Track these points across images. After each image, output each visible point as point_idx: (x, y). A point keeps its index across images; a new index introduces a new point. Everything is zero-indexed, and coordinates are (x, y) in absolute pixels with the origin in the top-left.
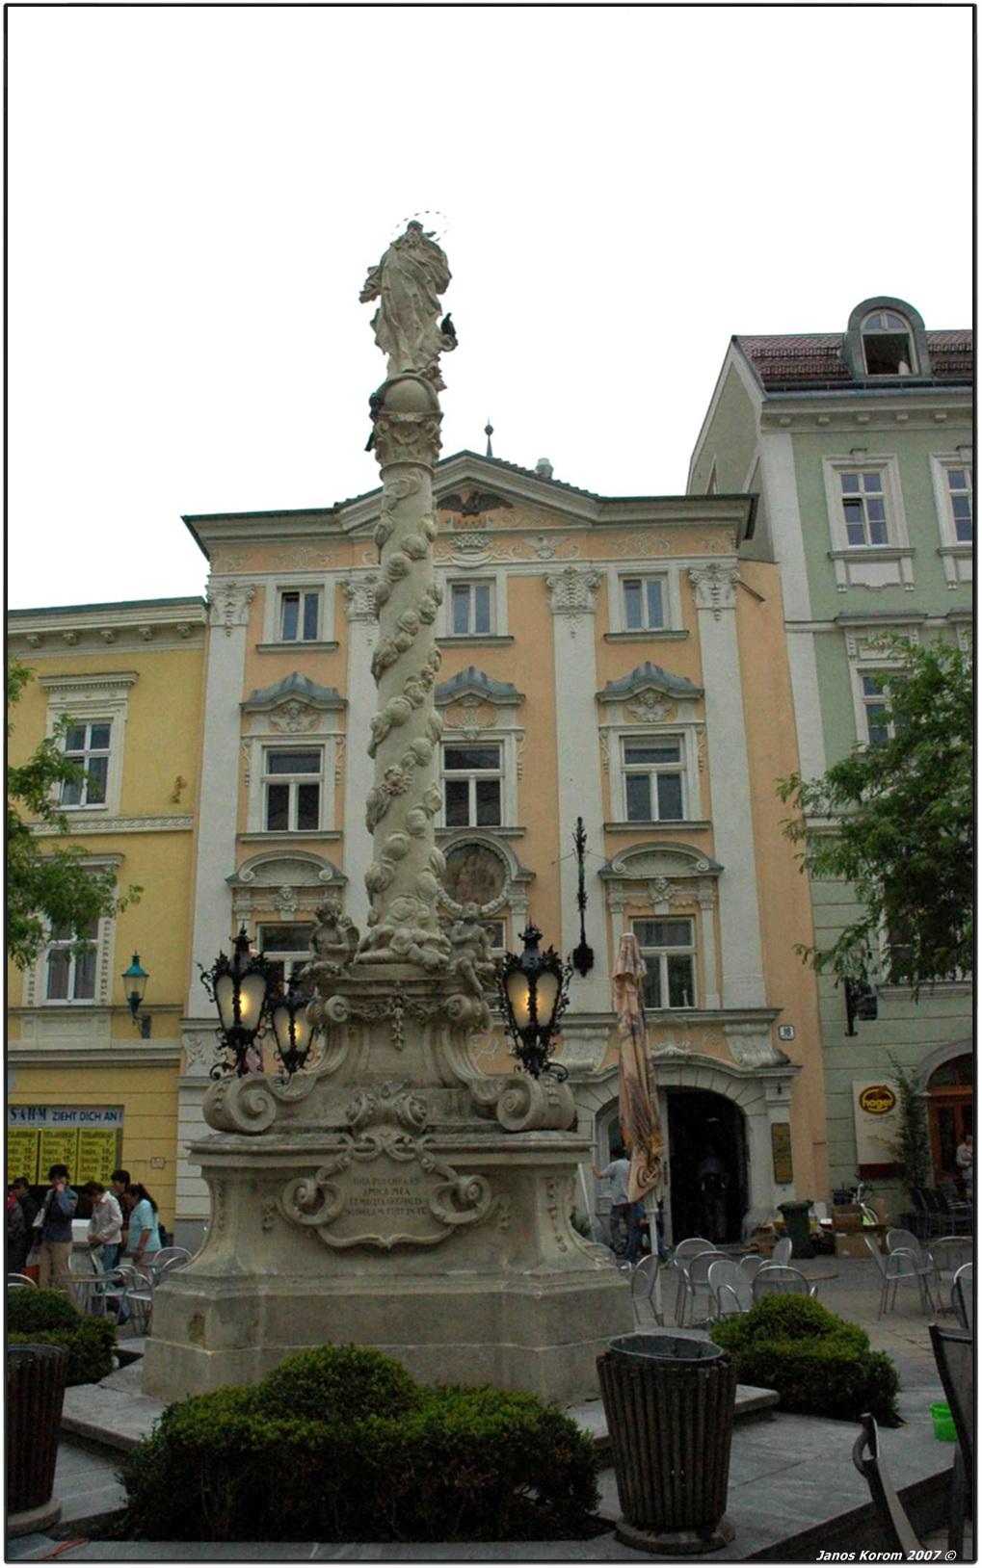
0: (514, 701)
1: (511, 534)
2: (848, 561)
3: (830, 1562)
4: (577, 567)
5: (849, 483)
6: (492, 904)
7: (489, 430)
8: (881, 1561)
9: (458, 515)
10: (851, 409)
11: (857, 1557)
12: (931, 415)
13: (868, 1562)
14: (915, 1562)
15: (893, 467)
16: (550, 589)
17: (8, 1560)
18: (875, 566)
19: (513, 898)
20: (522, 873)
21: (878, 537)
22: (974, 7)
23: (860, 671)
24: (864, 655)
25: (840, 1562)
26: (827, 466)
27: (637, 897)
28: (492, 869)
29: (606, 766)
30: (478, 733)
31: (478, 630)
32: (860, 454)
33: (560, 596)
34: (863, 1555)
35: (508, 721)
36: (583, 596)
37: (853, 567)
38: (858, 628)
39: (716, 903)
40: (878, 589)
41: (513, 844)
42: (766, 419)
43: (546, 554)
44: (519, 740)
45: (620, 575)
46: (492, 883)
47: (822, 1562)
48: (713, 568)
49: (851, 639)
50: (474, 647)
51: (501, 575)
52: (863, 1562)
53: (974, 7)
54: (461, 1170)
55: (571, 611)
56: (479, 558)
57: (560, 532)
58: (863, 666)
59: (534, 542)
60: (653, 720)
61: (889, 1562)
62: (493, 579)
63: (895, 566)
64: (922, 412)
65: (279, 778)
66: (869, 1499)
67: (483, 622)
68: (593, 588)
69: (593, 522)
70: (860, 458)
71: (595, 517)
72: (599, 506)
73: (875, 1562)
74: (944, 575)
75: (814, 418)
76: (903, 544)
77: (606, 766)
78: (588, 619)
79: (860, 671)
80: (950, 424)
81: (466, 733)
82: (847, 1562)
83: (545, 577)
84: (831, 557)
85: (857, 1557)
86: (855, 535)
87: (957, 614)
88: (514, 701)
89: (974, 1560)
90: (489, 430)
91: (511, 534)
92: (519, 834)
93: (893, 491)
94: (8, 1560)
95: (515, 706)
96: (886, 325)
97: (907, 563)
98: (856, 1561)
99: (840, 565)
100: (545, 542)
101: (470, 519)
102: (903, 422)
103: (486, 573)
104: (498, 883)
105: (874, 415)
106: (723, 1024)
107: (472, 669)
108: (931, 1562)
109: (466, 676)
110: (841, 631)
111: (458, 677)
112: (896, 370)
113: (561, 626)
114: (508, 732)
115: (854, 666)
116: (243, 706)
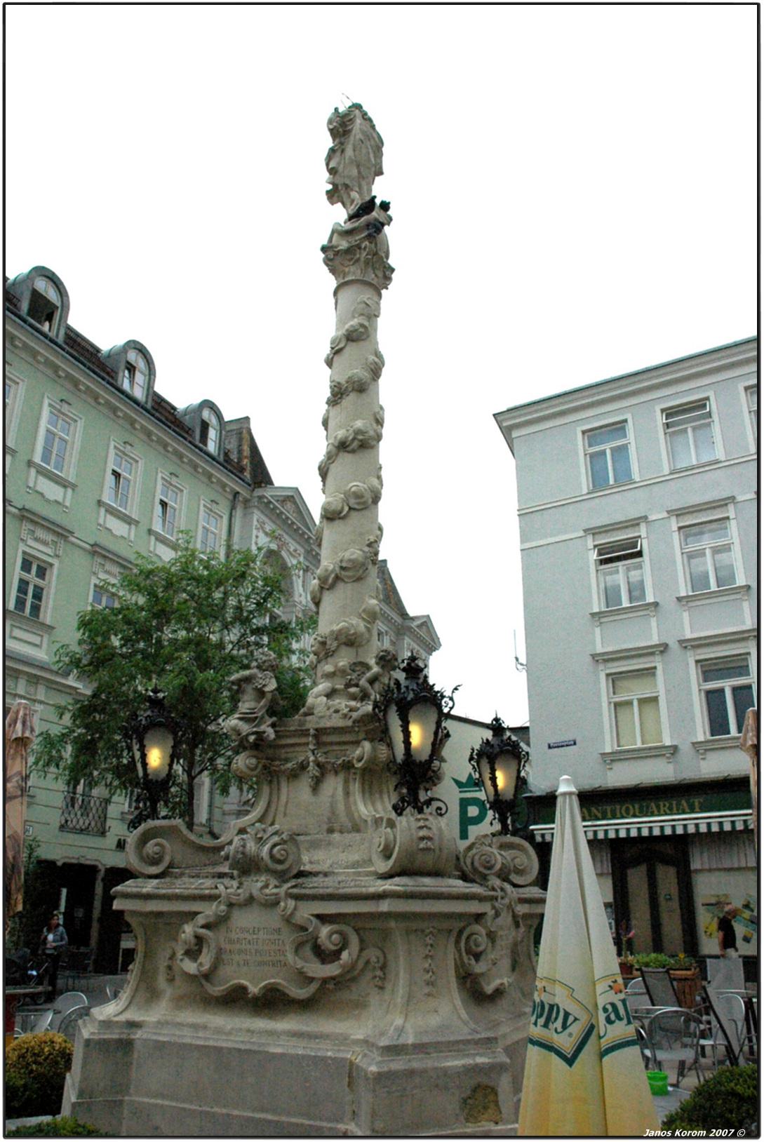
8: (691, 1137)
10: (16, 333)
12: (56, 369)
13: (681, 1137)
14: (715, 1137)
18: (52, 484)
21: (59, 466)
22: (758, 5)
23: (24, 553)
32: (66, 406)
34: (677, 1133)
37: (41, 478)
40: (48, 501)
52: (677, 1137)
53: (758, 5)
54: (323, 918)
61: (696, 1137)
63: (127, 526)
73: (686, 1137)
74: (27, 479)
76: (72, 479)
79: (24, 553)
85: (673, 1133)
86: (46, 456)
87: (27, 510)
89: (758, 1136)
97: (70, 491)
98: (673, 1137)
99: (33, 471)
102: (38, 362)
105: (26, 346)
108: (727, 1137)
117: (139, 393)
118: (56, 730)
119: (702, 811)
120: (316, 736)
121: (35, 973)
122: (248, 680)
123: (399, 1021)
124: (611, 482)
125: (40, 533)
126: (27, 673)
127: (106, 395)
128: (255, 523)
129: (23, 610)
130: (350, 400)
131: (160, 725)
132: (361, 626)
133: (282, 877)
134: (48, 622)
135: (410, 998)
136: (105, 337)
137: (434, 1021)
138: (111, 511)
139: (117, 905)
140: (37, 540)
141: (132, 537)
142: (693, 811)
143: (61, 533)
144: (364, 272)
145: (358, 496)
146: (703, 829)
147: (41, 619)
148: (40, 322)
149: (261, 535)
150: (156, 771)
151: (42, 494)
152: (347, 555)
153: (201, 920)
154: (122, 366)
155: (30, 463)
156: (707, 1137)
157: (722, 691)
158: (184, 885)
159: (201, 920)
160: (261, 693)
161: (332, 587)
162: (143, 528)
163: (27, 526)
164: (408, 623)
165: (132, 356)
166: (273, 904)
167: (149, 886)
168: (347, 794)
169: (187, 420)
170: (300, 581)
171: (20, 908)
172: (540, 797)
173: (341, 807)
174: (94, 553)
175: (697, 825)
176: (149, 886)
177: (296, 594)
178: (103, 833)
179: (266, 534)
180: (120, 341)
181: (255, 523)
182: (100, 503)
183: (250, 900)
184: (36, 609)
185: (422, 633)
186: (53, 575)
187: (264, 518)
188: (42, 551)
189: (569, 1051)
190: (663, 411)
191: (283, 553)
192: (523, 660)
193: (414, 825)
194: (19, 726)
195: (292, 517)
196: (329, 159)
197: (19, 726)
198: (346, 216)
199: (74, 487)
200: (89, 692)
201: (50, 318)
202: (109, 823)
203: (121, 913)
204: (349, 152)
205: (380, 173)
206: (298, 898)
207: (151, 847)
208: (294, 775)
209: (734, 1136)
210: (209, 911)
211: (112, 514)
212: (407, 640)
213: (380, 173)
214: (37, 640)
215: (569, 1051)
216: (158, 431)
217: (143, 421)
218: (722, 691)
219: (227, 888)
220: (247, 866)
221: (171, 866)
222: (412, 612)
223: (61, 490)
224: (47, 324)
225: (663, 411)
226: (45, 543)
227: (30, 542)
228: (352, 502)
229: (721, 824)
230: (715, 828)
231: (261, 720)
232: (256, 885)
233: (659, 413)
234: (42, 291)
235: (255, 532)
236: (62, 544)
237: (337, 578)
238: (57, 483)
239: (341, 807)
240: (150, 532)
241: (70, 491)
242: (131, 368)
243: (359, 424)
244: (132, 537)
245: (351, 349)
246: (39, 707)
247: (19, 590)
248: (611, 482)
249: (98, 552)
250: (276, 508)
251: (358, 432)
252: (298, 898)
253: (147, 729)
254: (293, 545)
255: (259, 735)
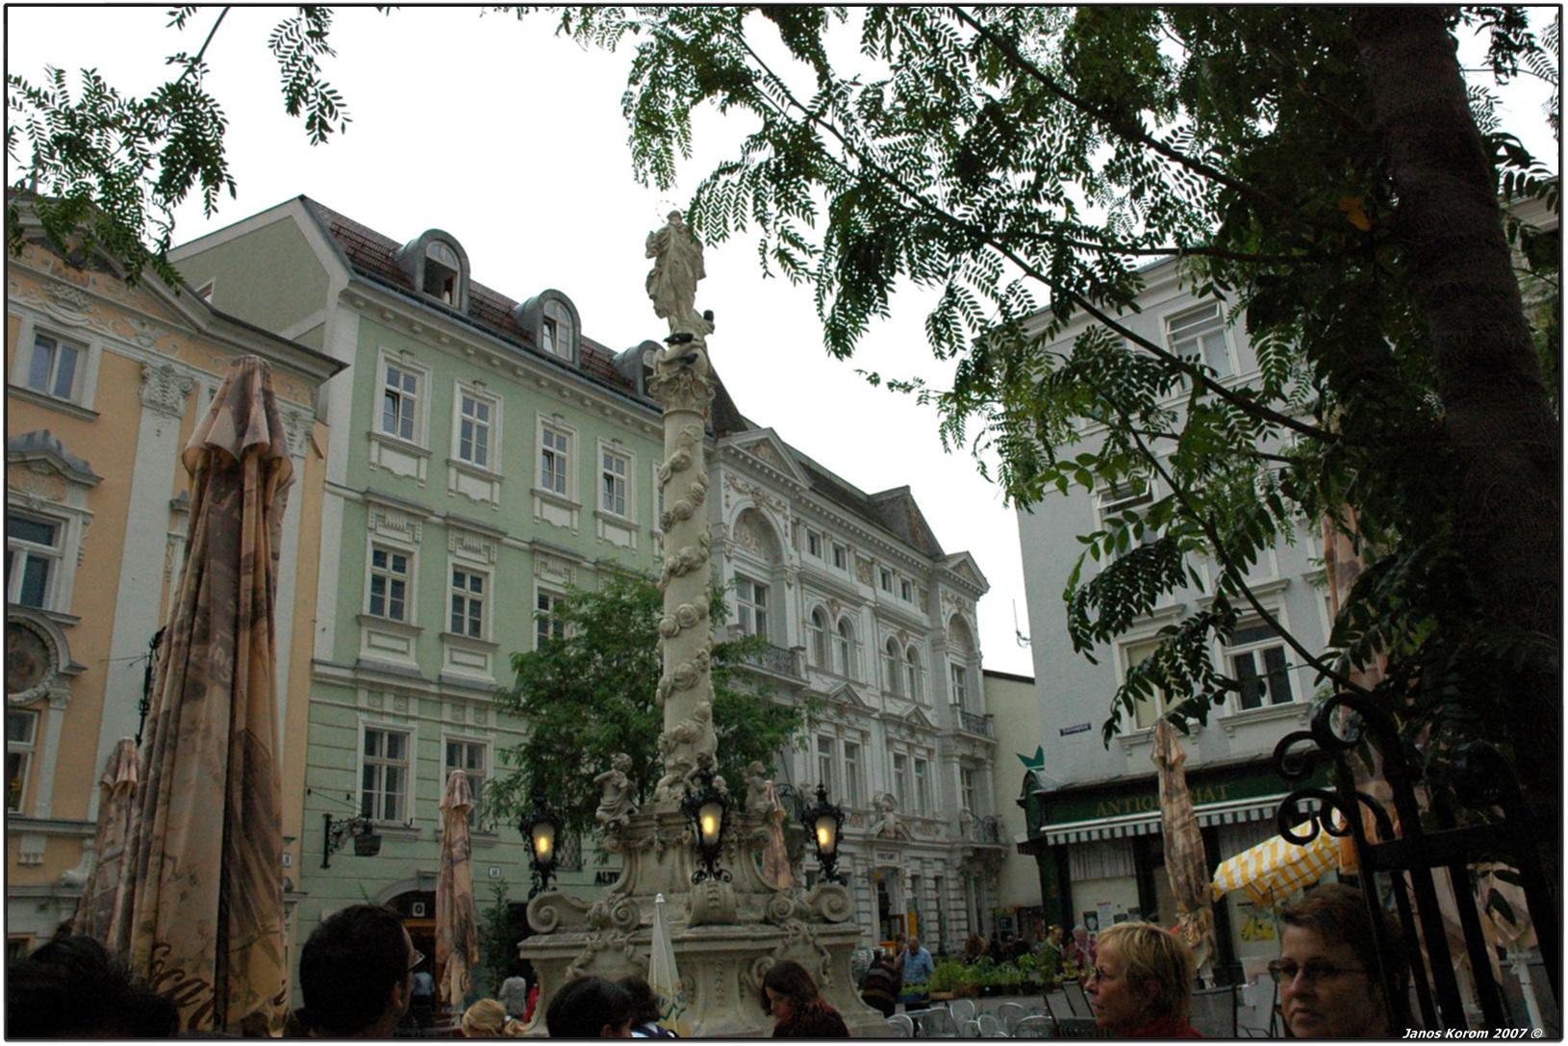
0: (88, 482)
1: (108, 304)
2: (382, 445)
4: (174, 366)
5: (393, 378)
6: (28, 693)
9: (60, 262)
10: (382, 304)
13: (1454, 1040)
15: (428, 376)
16: (144, 379)
19: (54, 691)
20: (73, 666)
21: (481, 459)
24: (381, 531)
26: (381, 356)
28: (34, 654)
29: (168, 573)
30: (43, 504)
31: (57, 392)
32: (407, 357)
33: (152, 389)
35: (76, 500)
36: (174, 394)
37: (462, 477)
38: (381, 505)
40: (475, 502)
41: (67, 633)
42: (346, 295)
43: (145, 341)
44: (85, 524)
45: (36, 328)
46: (32, 669)
48: (166, 371)
49: (373, 511)
50: (37, 404)
51: (97, 345)
52: (1449, 1040)
55: (162, 408)
56: (75, 318)
57: (163, 325)
58: (378, 540)
59: (135, 324)
60: (40, 493)
61: (1475, 1040)
62: (86, 346)
64: (405, 319)
67: (64, 387)
68: (186, 394)
69: (199, 329)
70: (407, 359)
71: (204, 326)
72: (212, 318)
73: (1461, 1040)
75: (381, 311)
76: (424, 445)
77: (168, 573)
78: (176, 422)
80: (448, 349)
81: (28, 500)
83: (142, 366)
84: (370, 436)
86: (465, 452)
88: (88, 482)
91: (108, 304)
92: (67, 623)
93: (424, 397)
95: (89, 486)
96: (444, 257)
97: (424, 461)
99: (453, 472)
100: (147, 329)
101: (72, 272)
103: (78, 335)
104: (38, 669)
106: (83, 837)
107: (47, 433)
109: (38, 438)
110: (367, 504)
111: (31, 436)
112: (439, 296)
113: (149, 421)
114: (77, 512)
115: (451, 560)
116: (172, 504)
117: (564, 353)
118: (503, 777)
119: (1230, 799)
120: (659, 820)
122: (607, 779)
123: (697, 1023)
125: (469, 540)
126: (477, 701)
127: (524, 363)
128: (723, 480)
129: (461, 630)
130: (678, 526)
131: (542, 822)
132: (694, 727)
133: (626, 929)
134: (490, 639)
135: (706, 1006)
136: (519, 288)
137: (722, 1022)
138: (547, 500)
139: (523, 955)
140: (467, 548)
141: (576, 525)
142: (1218, 800)
143: (492, 536)
144: (684, 401)
145: (687, 616)
146: (1229, 820)
147: (483, 637)
148: (439, 296)
149: (733, 493)
150: (544, 855)
151: (466, 496)
152: (679, 669)
153: (576, 963)
154: (540, 320)
155: (448, 462)
157: (1249, 656)
158: (562, 939)
159: (576, 963)
160: (617, 789)
161: (670, 695)
162: (587, 510)
163: (454, 535)
164: (939, 566)
165: (551, 310)
166: (619, 949)
167: (543, 941)
168: (682, 863)
169: (627, 373)
170: (789, 541)
171: (476, 959)
172: (1052, 794)
173: (678, 873)
174: (533, 552)
175: (1222, 816)
176: (543, 941)
177: (785, 557)
178: (579, 869)
179: (739, 491)
180: (535, 292)
181: (723, 480)
182: (533, 492)
183: (606, 947)
184: (476, 627)
185: (963, 575)
186: (490, 585)
187: (733, 472)
188: (474, 561)
190: (1167, 319)
191: (764, 510)
192: (1026, 633)
193: (707, 890)
194: (457, 795)
195: (770, 465)
196: (648, 285)
197: (457, 795)
198: (668, 334)
199: (500, 479)
200: (868, 231)
201: (449, 287)
202: (584, 856)
203: (527, 961)
204: (666, 276)
205: (703, 276)
206: (636, 944)
207: (543, 913)
208: (645, 851)
210: (581, 956)
211: (550, 503)
212: (942, 587)
213: (703, 276)
214: (480, 661)
216: (593, 395)
217: (574, 386)
218: (1249, 656)
219: (594, 939)
220: (603, 923)
221: (558, 924)
222: (948, 549)
223: (486, 487)
224: (447, 295)
225: (1167, 319)
226: (477, 551)
227: (460, 553)
228: (682, 622)
229: (1247, 813)
230: (1242, 818)
231: (619, 809)
232: (608, 936)
233: (1162, 322)
234: (436, 259)
235: (723, 491)
236: (495, 547)
237: (674, 688)
238: (482, 479)
239: (678, 873)
240: (596, 514)
241: (497, 486)
242: (551, 324)
243: (684, 551)
244: (576, 525)
245: (677, 479)
246: (492, 736)
247: (455, 609)
249: (538, 550)
250: (746, 457)
251: (684, 559)
252: (636, 944)
253: (534, 824)
254: (775, 498)
255: (617, 822)
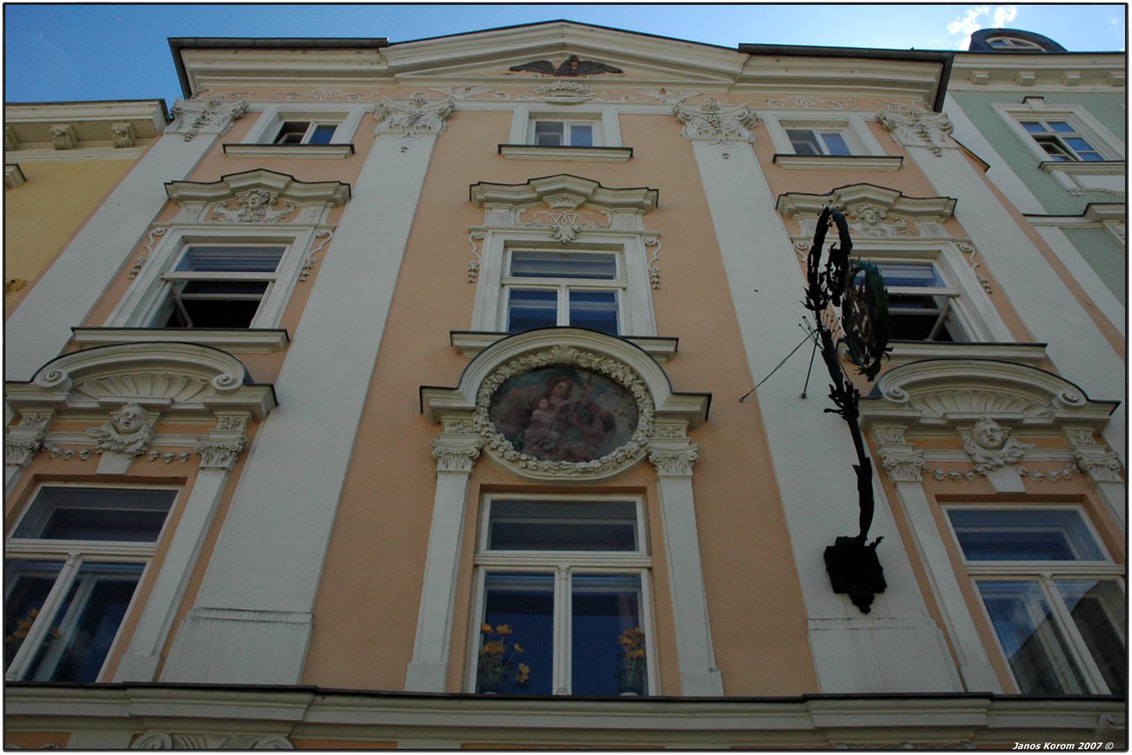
3: (1023, 751)
7: (804, 396)
8: (1059, 750)
11: (1077, 746)
13: (1050, 751)
14: (1084, 750)
17: (6, 749)
22: (1126, 5)
25: (1029, 750)
27: (944, 457)
34: (1046, 746)
39: (242, 454)
47: (1017, 750)
52: (1046, 750)
53: (1126, 5)
61: (1065, 750)
65: (36, 547)
66: (554, 693)
73: (1055, 750)
82: (1035, 750)
85: (1077, 746)
89: (1126, 749)
90: (804, 396)
94: (6, 749)
98: (1041, 750)
108: (1095, 750)
121: (517, 647)
124: (562, 680)
156: (1076, 750)
189: (426, 393)
209: (1102, 750)
215: (426, 393)
238: (109, 288)
248: (562, 680)
